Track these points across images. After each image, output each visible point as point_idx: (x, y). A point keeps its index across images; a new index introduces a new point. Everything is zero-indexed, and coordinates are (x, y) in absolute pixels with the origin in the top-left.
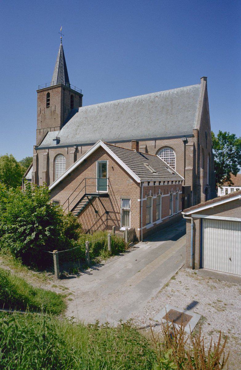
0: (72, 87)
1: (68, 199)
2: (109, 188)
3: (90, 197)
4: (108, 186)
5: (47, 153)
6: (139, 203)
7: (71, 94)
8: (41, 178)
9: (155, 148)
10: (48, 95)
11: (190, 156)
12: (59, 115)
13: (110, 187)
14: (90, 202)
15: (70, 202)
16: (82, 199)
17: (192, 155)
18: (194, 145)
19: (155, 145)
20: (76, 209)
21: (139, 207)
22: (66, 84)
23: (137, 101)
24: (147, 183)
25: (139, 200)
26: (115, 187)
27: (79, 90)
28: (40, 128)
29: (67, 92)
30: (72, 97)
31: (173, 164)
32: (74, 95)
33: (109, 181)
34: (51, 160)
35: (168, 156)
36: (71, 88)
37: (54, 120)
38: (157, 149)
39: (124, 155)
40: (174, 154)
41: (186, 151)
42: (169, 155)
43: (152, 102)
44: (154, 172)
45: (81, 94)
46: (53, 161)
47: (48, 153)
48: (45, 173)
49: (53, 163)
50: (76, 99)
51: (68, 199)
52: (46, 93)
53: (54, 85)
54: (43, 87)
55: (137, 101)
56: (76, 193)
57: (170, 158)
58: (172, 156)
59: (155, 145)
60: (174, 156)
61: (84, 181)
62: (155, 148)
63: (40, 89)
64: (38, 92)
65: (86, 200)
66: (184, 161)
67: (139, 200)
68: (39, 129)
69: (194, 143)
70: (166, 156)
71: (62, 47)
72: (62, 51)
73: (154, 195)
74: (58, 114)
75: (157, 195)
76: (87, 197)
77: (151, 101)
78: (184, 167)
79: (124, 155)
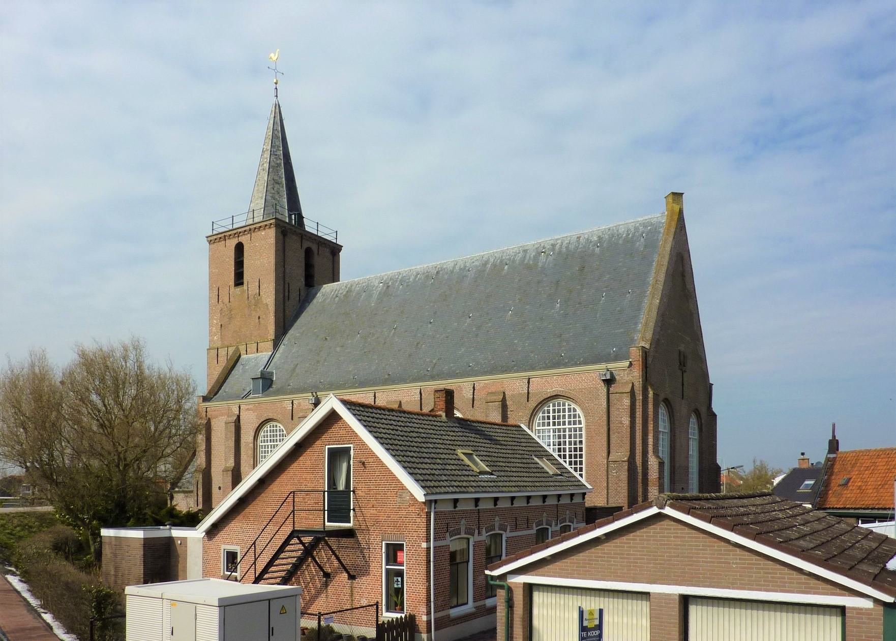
0: (310, 227)
1: (254, 543)
2: (355, 516)
3: (307, 539)
4: (354, 510)
5: (235, 418)
6: (424, 553)
7: (306, 244)
8: (220, 488)
9: (528, 401)
10: (240, 248)
11: (621, 422)
12: (272, 308)
13: (359, 514)
14: (308, 552)
15: (258, 551)
16: (286, 543)
17: (626, 421)
18: (632, 393)
19: (528, 393)
20: (273, 569)
21: (424, 563)
22: (290, 216)
23: (489, 266)
24: (569, 496)
25: (424, 545)
26: (370, 512)
27: (328, 231)
28: (219, 344)
29: (293, 243)
30: (308, 253)
31: (562, 447)
32: (314, 247)
33: (356, 498)
34: (247, 437)
35: (564, 424)
36: (307, 229)
37: (257, 320)
38: (533, 404)
39: (397, 430)
40: (579, 417)
41: (612, 409)
42: (551, 421)
43: (529, 267)
44: (481, 473)
45: (336, 244)
46: (251, 438)
47: (239, 417)
48: (230, 473)
49: (252, 445)
50: (320, 261)
51: (254, 543)
52: (233, 242)
53: (256, 220)
54: (224, 225)
55: (489, 266)
56: (272, 528)
57: (570, 430)
58: (575, 423)
59: (528, 393)
60: (580, 423)
61: (290, 499)
62: (528, 401)
63: (215, 232)
64: (210, 242)
65: (295, 550)
66: (605, 435)
67: (424, 545)
68: (215, 346)
69: (633, 385)
70: (559, 424)
71: (279, 106)
72: (278, 111)
73: (477, 531)
74: (267, 305)
75: (537, 527)
76: (299, 539)
77: (527, 264)
78: (605, 455)
79: (397, 430)
